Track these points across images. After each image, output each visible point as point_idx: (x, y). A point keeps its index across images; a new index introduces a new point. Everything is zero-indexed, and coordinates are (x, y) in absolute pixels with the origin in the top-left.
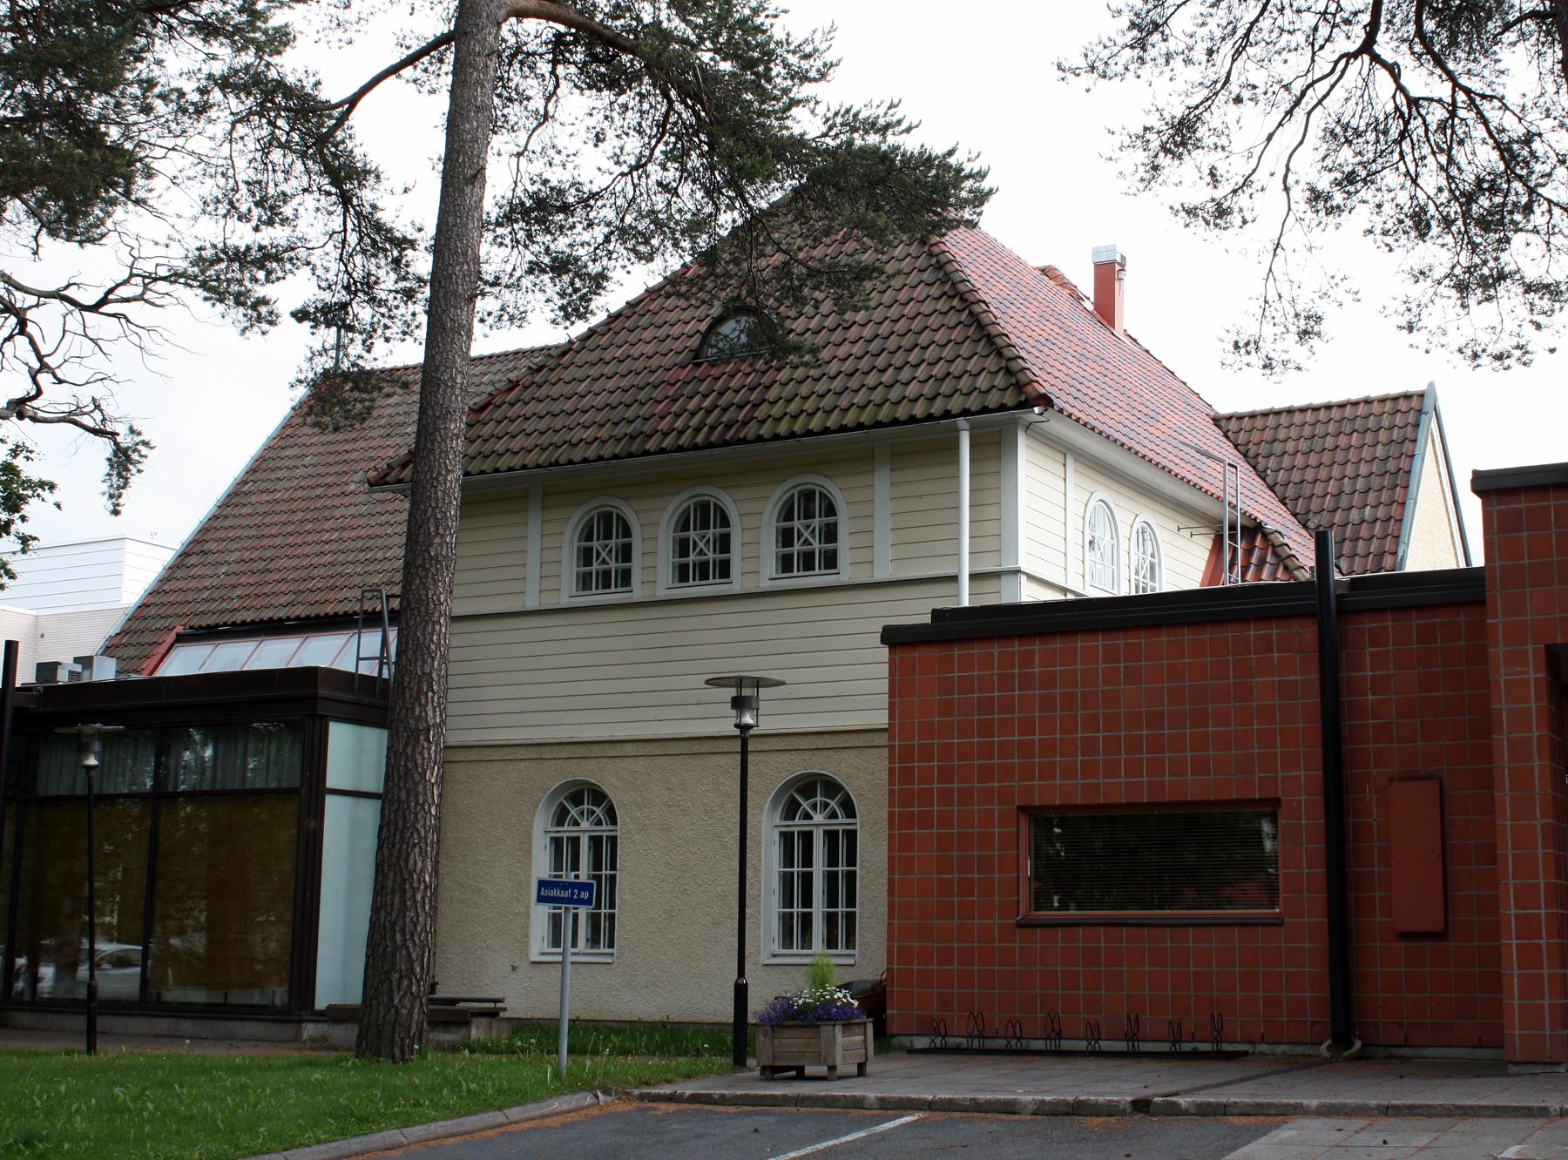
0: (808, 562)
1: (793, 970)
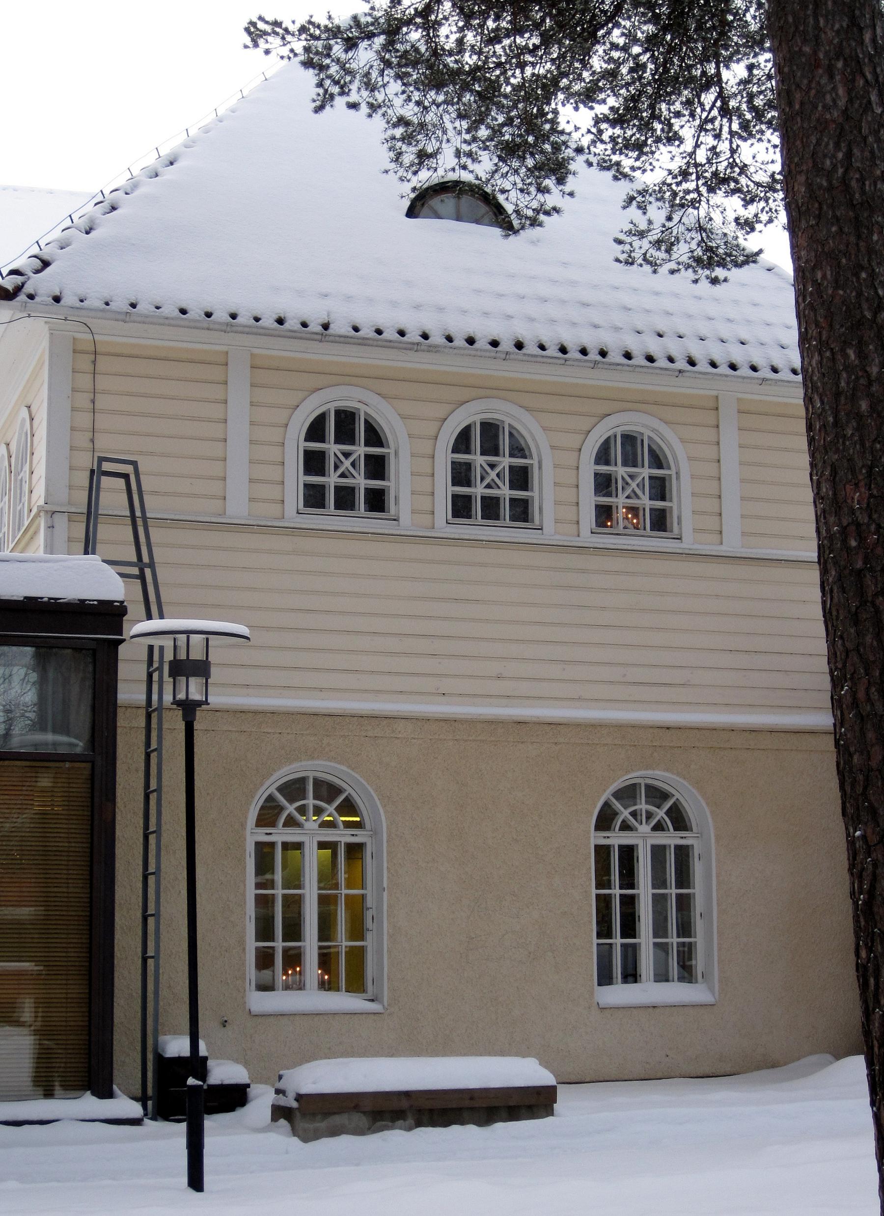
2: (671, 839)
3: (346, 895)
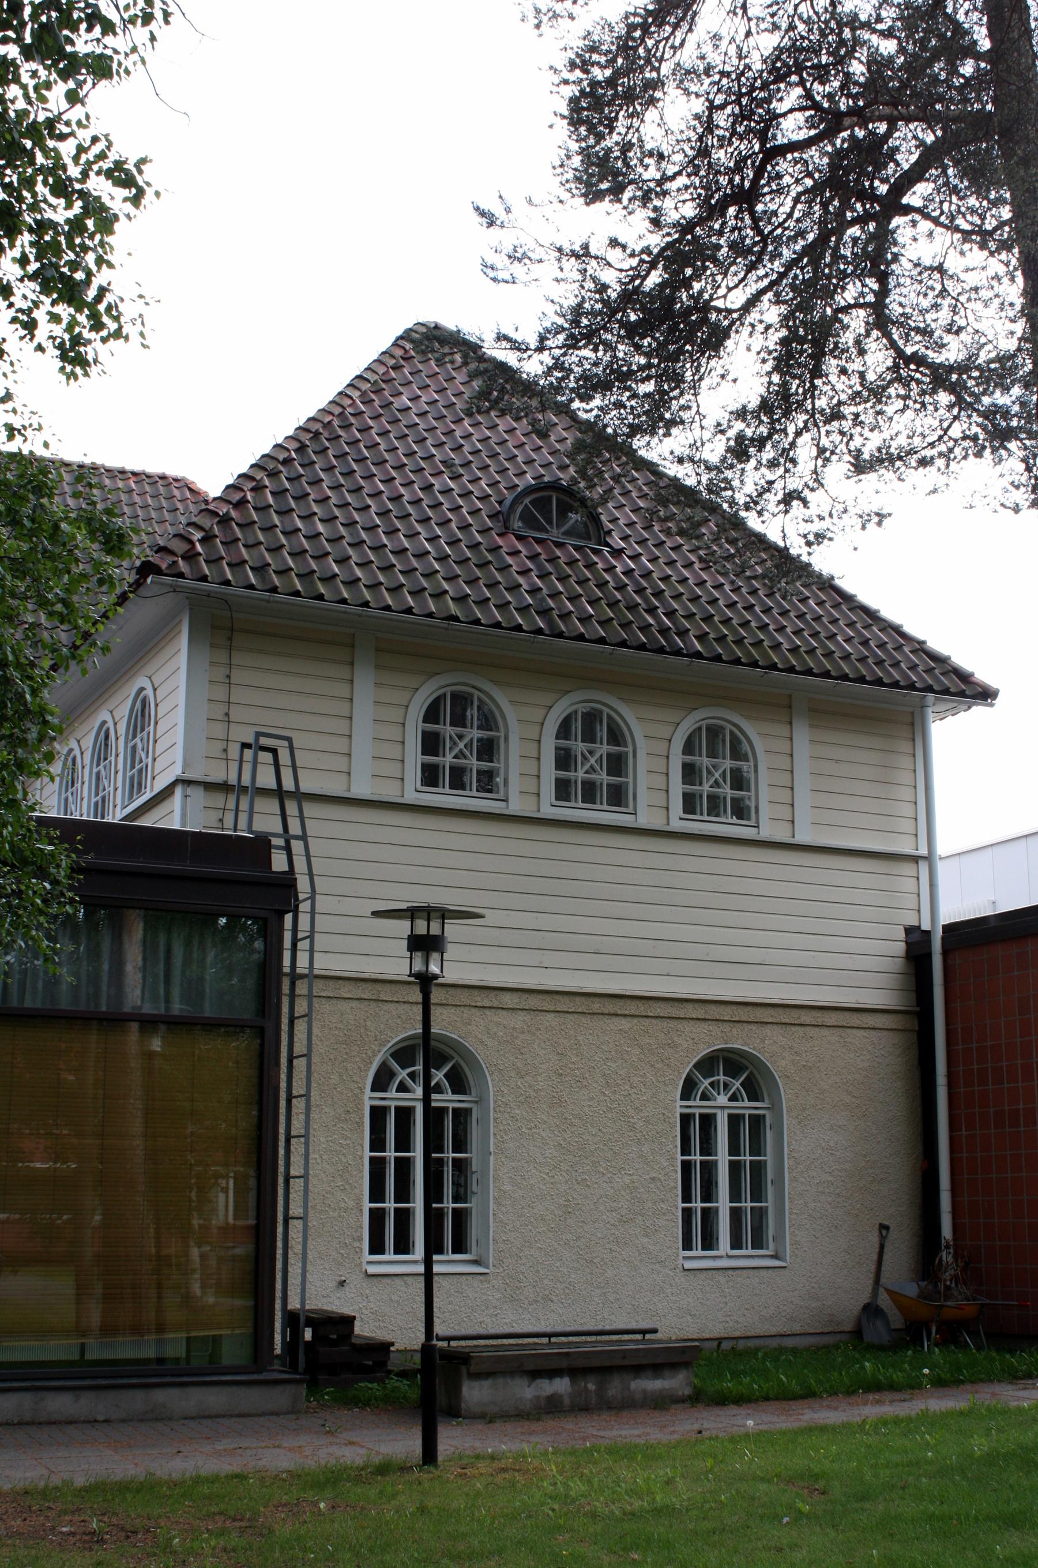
0: (715, 806)
1: (720, 1277)
2: (746, 1106)
3: (454, 1159)
